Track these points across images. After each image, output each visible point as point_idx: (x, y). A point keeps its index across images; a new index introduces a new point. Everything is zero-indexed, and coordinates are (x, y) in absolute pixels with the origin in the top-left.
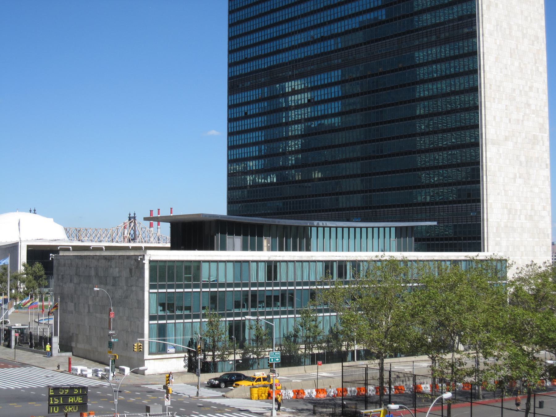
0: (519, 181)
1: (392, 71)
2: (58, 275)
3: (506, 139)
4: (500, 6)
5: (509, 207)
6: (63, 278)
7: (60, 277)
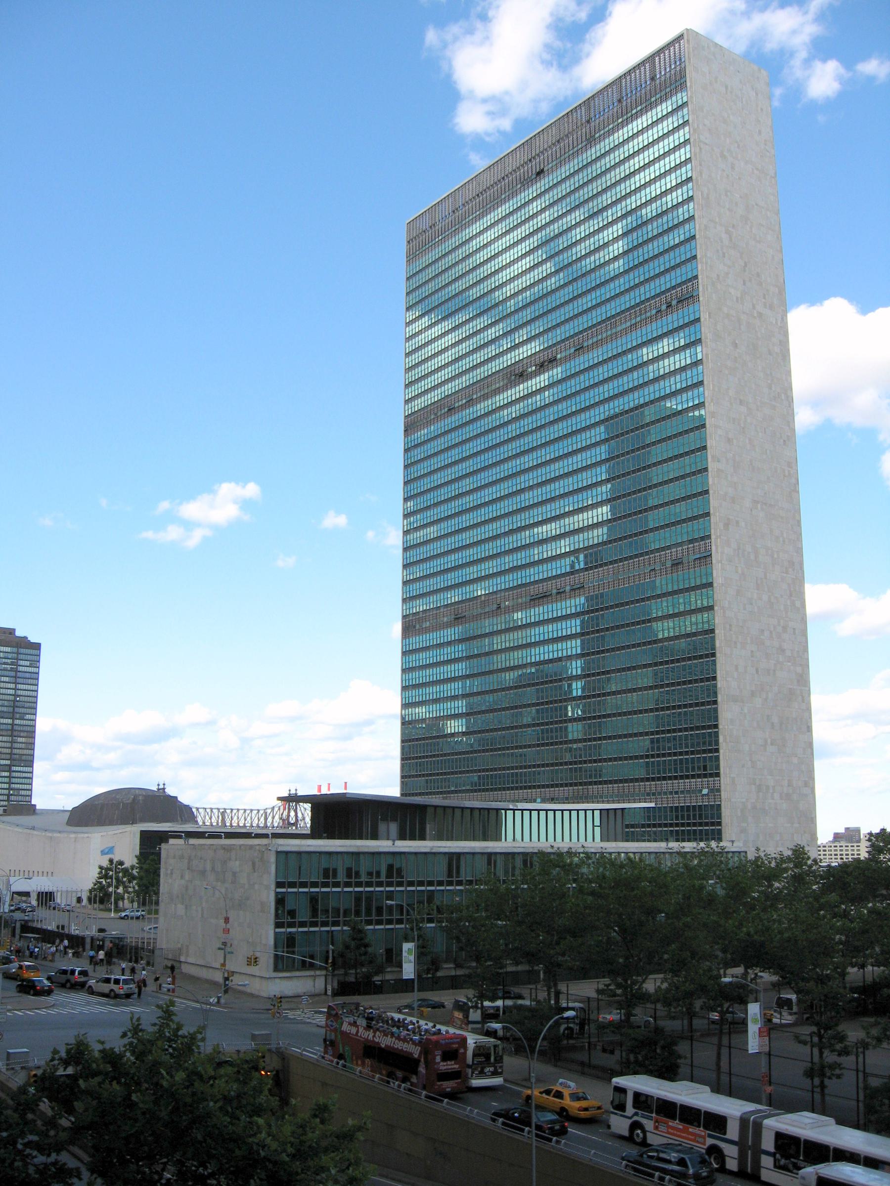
0: (771, 749)
1: (617, 606)
2: (167, 869)
3: (753, 694)
4: (743, 524)
5: (758, 782)
6: (172, 874)
7: (169, 872)
